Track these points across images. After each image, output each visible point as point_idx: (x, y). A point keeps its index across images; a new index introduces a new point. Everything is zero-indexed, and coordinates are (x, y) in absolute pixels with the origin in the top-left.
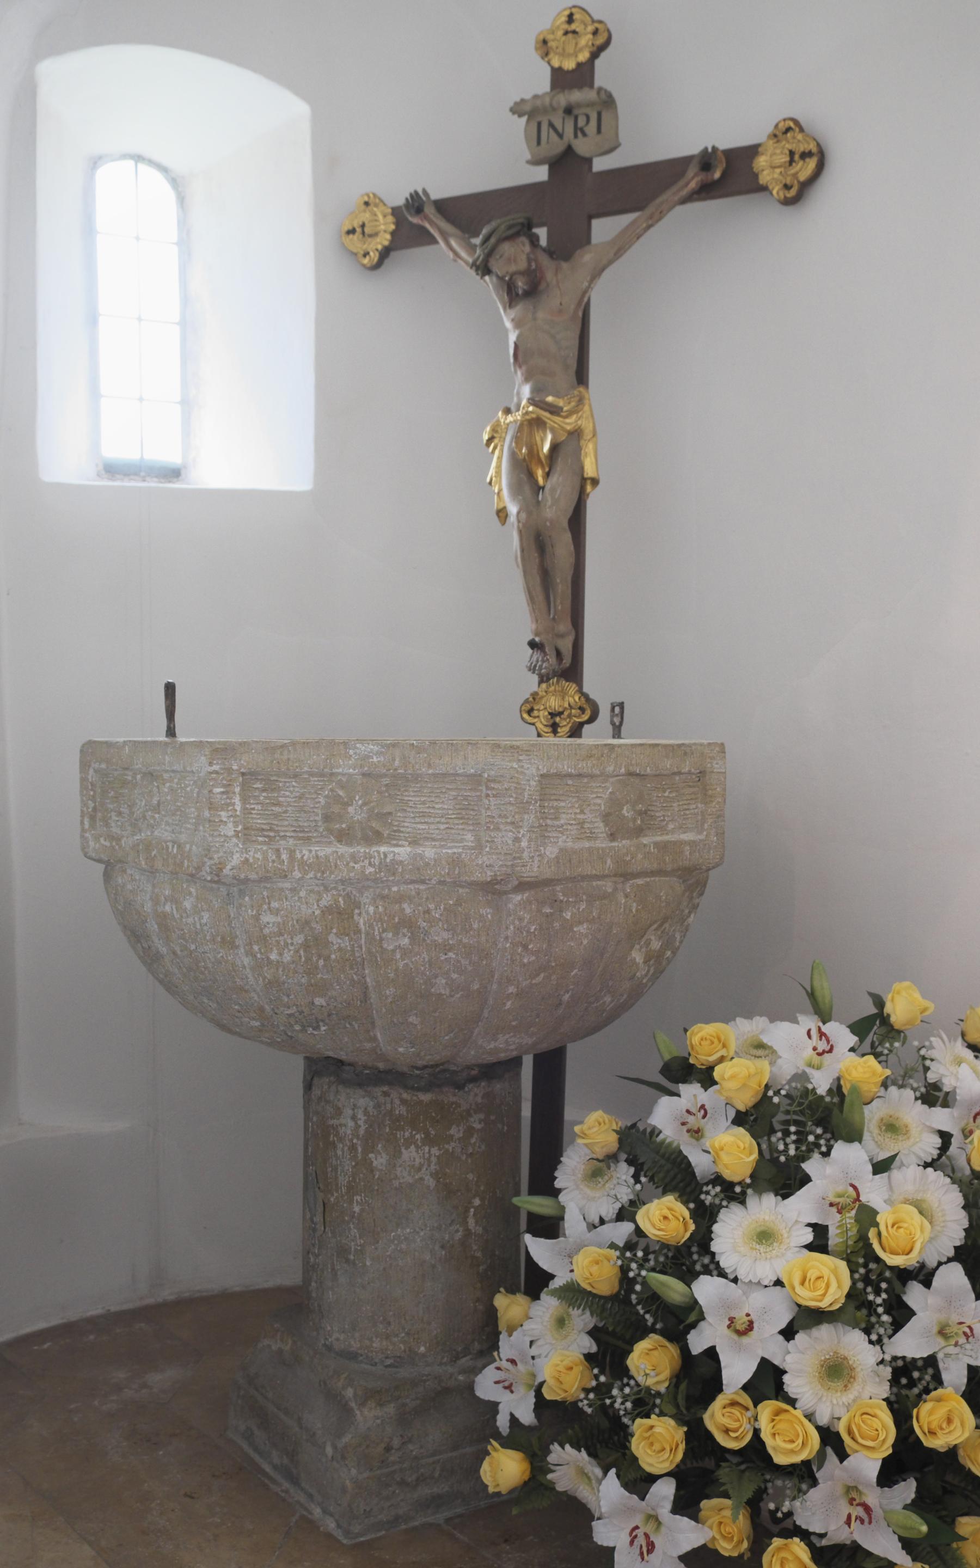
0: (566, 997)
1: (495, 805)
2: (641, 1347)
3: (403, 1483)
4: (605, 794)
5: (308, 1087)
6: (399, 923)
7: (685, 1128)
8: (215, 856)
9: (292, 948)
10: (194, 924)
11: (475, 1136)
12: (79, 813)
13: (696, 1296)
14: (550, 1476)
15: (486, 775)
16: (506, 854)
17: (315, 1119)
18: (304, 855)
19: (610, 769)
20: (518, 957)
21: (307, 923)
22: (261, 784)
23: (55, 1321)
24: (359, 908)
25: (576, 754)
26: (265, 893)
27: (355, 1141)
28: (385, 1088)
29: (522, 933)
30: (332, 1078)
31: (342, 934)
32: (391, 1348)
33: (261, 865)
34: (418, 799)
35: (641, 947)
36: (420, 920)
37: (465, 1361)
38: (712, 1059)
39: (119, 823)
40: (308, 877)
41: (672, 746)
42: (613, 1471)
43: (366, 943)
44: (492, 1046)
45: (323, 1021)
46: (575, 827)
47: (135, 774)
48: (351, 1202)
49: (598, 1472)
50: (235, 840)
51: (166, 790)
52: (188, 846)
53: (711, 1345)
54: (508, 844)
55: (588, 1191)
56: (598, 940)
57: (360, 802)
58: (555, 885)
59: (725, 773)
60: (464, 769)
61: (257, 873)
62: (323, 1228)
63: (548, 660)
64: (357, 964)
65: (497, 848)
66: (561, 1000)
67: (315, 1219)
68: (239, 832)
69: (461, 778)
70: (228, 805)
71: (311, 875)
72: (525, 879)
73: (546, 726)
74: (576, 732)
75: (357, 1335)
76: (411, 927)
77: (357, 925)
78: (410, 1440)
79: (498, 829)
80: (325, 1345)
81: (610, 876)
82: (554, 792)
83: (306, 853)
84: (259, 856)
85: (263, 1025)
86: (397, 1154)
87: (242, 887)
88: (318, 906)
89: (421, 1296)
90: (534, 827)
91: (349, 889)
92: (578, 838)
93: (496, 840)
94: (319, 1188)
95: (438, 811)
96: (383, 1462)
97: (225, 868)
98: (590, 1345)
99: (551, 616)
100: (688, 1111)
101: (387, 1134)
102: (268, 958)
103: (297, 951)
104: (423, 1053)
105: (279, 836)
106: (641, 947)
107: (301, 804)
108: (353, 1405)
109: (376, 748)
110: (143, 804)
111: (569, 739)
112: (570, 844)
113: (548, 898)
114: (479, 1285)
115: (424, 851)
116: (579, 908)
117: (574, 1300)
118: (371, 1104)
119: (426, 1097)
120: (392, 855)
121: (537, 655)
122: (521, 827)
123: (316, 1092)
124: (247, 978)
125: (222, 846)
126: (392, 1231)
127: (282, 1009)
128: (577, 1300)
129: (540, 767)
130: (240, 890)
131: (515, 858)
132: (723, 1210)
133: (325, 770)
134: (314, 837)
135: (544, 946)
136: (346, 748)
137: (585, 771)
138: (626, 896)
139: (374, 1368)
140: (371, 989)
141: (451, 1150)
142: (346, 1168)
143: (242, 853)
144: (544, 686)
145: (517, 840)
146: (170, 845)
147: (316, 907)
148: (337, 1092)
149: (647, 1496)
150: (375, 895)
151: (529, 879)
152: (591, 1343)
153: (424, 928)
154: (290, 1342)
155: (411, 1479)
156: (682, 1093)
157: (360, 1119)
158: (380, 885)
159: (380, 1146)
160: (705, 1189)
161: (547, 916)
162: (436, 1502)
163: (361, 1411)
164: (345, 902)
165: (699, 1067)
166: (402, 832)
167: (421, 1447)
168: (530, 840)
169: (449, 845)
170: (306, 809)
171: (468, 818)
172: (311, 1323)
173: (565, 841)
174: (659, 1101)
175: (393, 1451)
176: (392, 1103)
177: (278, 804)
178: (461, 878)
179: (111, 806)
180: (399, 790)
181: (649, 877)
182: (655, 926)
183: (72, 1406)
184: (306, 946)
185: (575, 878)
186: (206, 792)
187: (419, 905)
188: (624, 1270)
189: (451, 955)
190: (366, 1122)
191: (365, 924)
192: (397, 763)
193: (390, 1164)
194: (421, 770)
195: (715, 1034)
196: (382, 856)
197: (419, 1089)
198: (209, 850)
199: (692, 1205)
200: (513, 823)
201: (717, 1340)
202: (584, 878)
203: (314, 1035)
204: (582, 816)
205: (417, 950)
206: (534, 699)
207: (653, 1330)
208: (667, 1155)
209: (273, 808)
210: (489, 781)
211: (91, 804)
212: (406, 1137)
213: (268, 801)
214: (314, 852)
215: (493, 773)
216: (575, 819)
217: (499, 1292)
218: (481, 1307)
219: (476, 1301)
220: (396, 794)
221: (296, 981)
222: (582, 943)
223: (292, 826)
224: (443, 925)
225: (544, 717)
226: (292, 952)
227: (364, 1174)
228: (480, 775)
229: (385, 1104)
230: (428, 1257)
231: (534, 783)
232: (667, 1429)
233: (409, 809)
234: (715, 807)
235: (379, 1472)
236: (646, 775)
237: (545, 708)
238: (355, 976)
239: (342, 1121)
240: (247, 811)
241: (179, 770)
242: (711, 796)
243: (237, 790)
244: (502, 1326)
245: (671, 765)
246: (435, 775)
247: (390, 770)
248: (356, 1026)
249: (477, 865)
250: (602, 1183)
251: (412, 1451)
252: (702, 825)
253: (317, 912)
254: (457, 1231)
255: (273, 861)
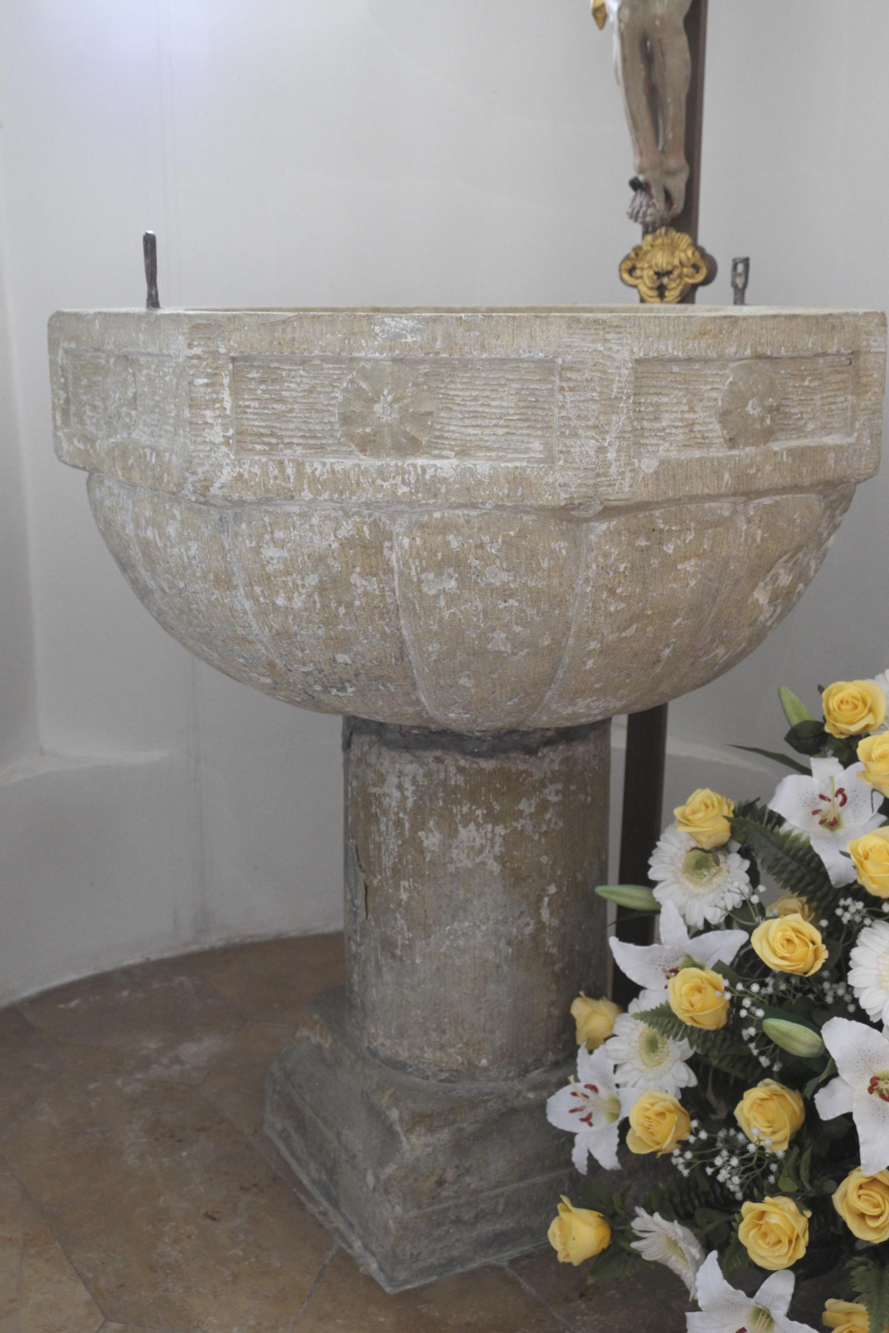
0: (667, 652)
1: (571, 402)
2: (752, 1095)
3: (458, 1221)
4: (724, 385)
5: (347, 745)
6: (442, 559)
7: (818, 818)
8: (200, 470)
9: (303, 591)
10: (181, 556)
11: (551, 810)
12: (50, 406)
13: (828, 1046)
14: (634, 1245)
15: (560, 361)
16: (586, 469)
17: (354, 784)
18: (316, 469)
19: (731, 350)
20: (602, 605)
21: (322, 559)
22: (258, 372)
23: (87, 972)
24: (391, 539)
25: (684, 330)
26: (267, 519)
27: (401, 815)
28: (438, 753)
29: (608, 574)
30: (374, 737)
31: (369, 573)
32: (445, 1059)
33: (260, 482)
34: (467, 393)
35: (766, 585)
36: (471, 557)
37: (536, 1075)
38: (854, 729)
39: (94, 420)
40: (322, 498)
41: (815, 317)
42: (714, 1254)
43: (399, 584)
44: (570, 710)
45: (349, 681)
46: (682, 431)
47: (109, 357)
48: (397, 887)
49: (695, 1251)
50: (224, 449)
51: (143, 379)
52: (167, 455)
53: (845, 1111)
54: (589, 456)
55: (691, 886)
56: (710, 580)
57: (390, 398)
58: (652, 509)
59: (885, 353)
60: (530, 352)
61: (255, 493)
62: (364, 914)
63: (654, 204)
64: (388, 613)
65: (574, 461)
66: (659, 656)
67: (356, 902)
68: (229, 438)
69: (526, 365)
70: (215, 401)
71: (326, 496)
72: (611, 503)
73: (651, 289)
74: (687, 296)
75: (406, 1042)
76: (459, 566)
77: (387, 562)
78: (467, 1171)
79: (574, 435)
80: (368, 1048)
81: (728, 495)
82: (654, 383)
83: (318, 466)
84: (256, 470)
85: (276, 683)
86: (453, 833)
87: (238, 510)
88: (336, 537)
89: (483, 1001)
90: (625, 432)
91: (377, 514)
92: (686, 446)
93: (572, 450)
94: (360, 866)
95: (494, 410)
96: (434, 1198)
97: (212, 486)
98: (689, 1078)
99: (660, 148)
100: (822, 797)
101: (440, 808)
102: (274, 603)
103: (310, 596)
104: (480, 720)
105: (283, 443)
106: (766, 585)
107: (311, 400)
108: (398, 1129)
109: (411, 324)
110: (117, 396)
111: (679, 306)
112: (674, 454)
113: (644, 527)
114: (554, 987)
115: (475, 465)
116: (685, 540)
117: (670, 1026)
118: (421, 771)
119: (488, 765)
120: (432, 470)
121: (641, 198)
122: (607, 432)
123: (356, 752)
124: (250, 626)
125: (208, 456)
126: (447, 925)
127: (296, 666)
128: (673, 1027)
129: (635, 349)
130: (236, 514)
131: (598, 475)
132: (865, 931)
133: (343, 354)
134: (329, 445)
135: (638, 590)
136: (370, 324)
137: (697, 353)
138: (749, 521)
139: (425, 1082)
140: (409, 643)
141: (520, 828)
142: (391, 847)
143: (235, 466)
144: (649, 238)
145: (601, 450)
146: (148, 451)
147: (332, 538)
148: (380, 754)
149: (758, 1293)
150: (410, 522)
151: (615, 503)
152: (689, 1075)
153: (476, 567)
154: (330, 1039)
155: (468, 1215)
156: (814, 771)
157: (407, 789)
158: (417, 510)
159: (432, 822)
160: (842, 902)
161: (642, 551)
162: (499, 1240)
163: (408, 1139)
164: (371, 532)
165: (837, 736)
166: (447, 438)
167: (481, 1179)
168: (619, 450)
169: (509, 456)
170: (318, 406)
171: (535, 420)
172: (354, 1020)
173: (667, 450)
174: (784, 780)
175: (446, 1185)
176: (446, 771)
177: (282, 400)
178: (526, 502)
179: (84, 398)
180: (443, 381)
181: (779, 494)
182: (785, 558)
183: (92, 1086)
184: (321, 589)
185: (680, 499)
186: (185, 383)
187: (470, 537)
188: (735, 1004)
189: (512, 602)
190: (414, 792)
191: (398, 562)
192: (439, 345)
193: (444, 845)
194: (471, 353)
195: (859, 697)
196: (420, 471)
197: (480, 755)
198: (191, 462)
199: (824, 923)
200: (596, 427)
201: (854, 1105)
202: (692, 499)
203: (340, 697)
204: (690, 416)
205: (466, 596)
206: (637, 255)
207: (767, 1073)
208: (792, 852)
209: (275, 406)
210: (563, 368)
211: (62, 395)
212: (464, 812)
213: (267, 396)
214: (328, 466)
215: (569, 357)
216: (681, 420)
217: (579, 996)
218: (556, 1012)
219: (550, 1006)
220: (438, 387)
221: (310, 632)
222: (688, 584)
223: (300, 430)
224: (501, 564)
225: (648, 277)
226: (304, 596)
227: (412, 856)
228: (552, 361)
229: (438, 772)
230: (490, 955)
231: (625, 372)
232: (785, 1217)
233: (456, 408)
234: (870, 400)
235: (429, 1209)
236: (781, 358)
237: (650, 267)
238: (386, 628)
239: (386, 790)
240: (240, 410)
241: (154, 352)
242: (865, 385)
243: (226, 381)
244: (581, 1039)
245: (814, 344)
246: (490, 361)
247: (428, 353)
248: (392, 689)
249: (547, 484)
250: (708, 877)
251: (469, 1184)
252: (852, 424)
253: (335, 545)
254: (528, 924)
255: (276, 478)
